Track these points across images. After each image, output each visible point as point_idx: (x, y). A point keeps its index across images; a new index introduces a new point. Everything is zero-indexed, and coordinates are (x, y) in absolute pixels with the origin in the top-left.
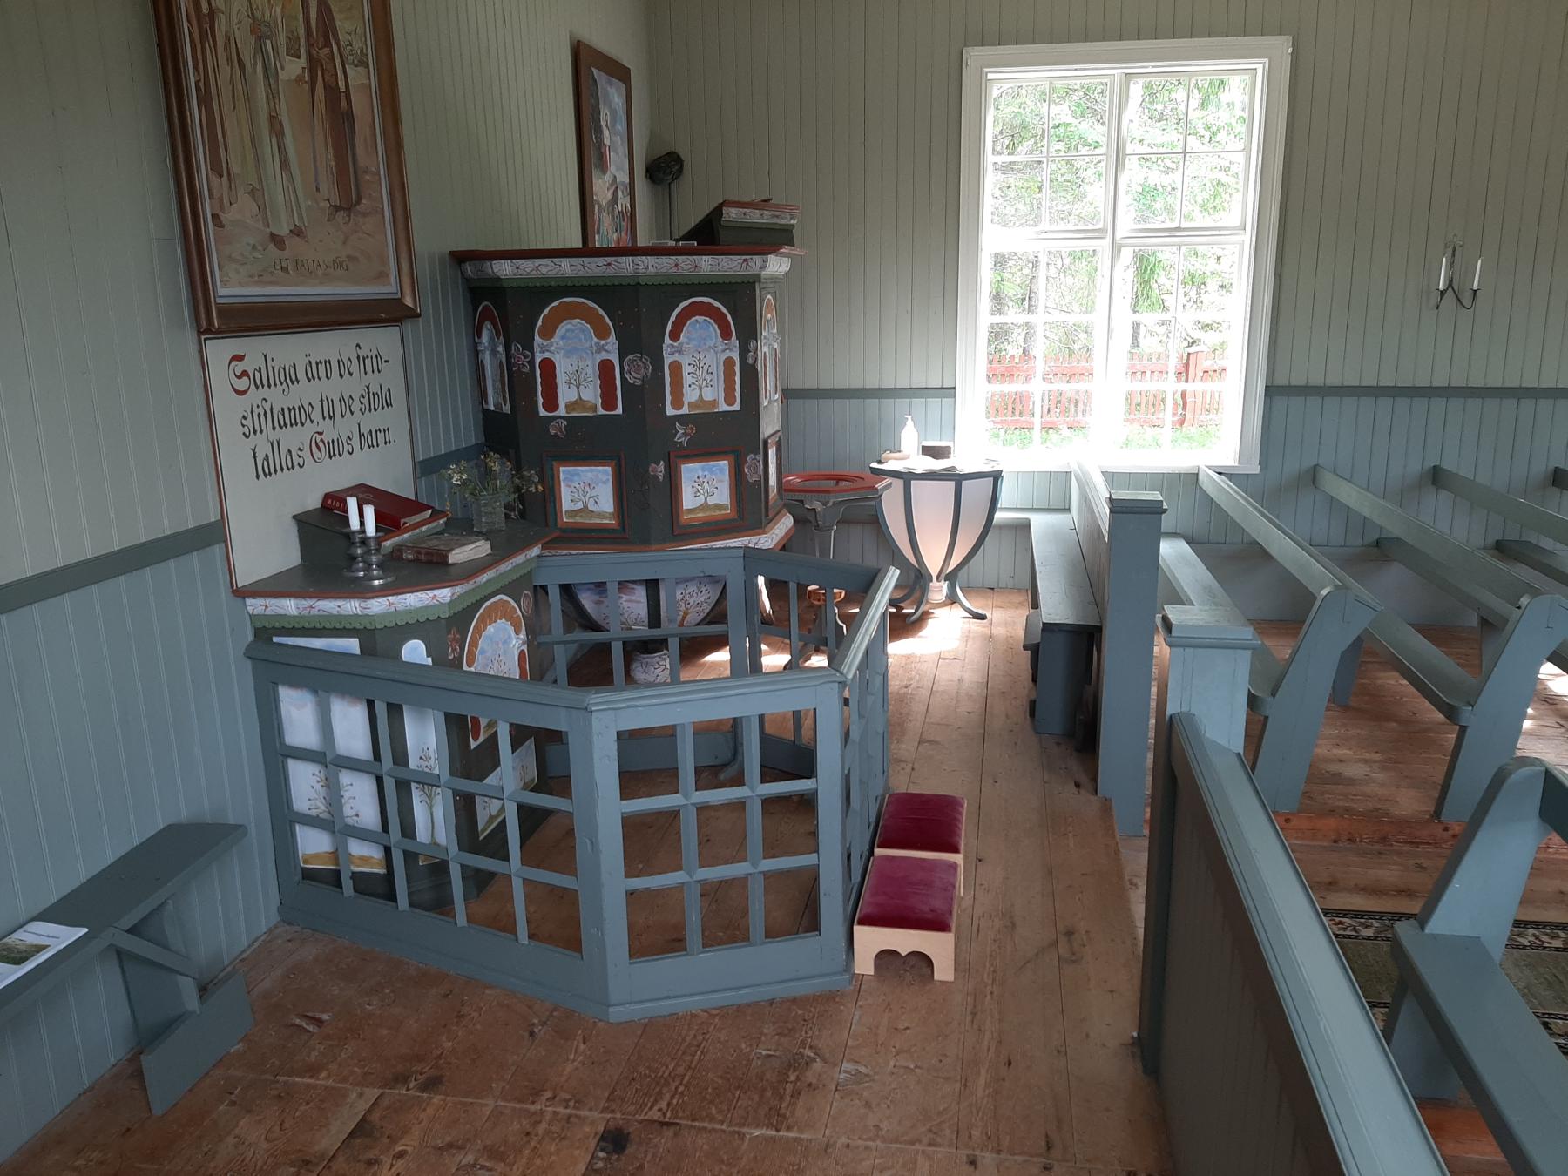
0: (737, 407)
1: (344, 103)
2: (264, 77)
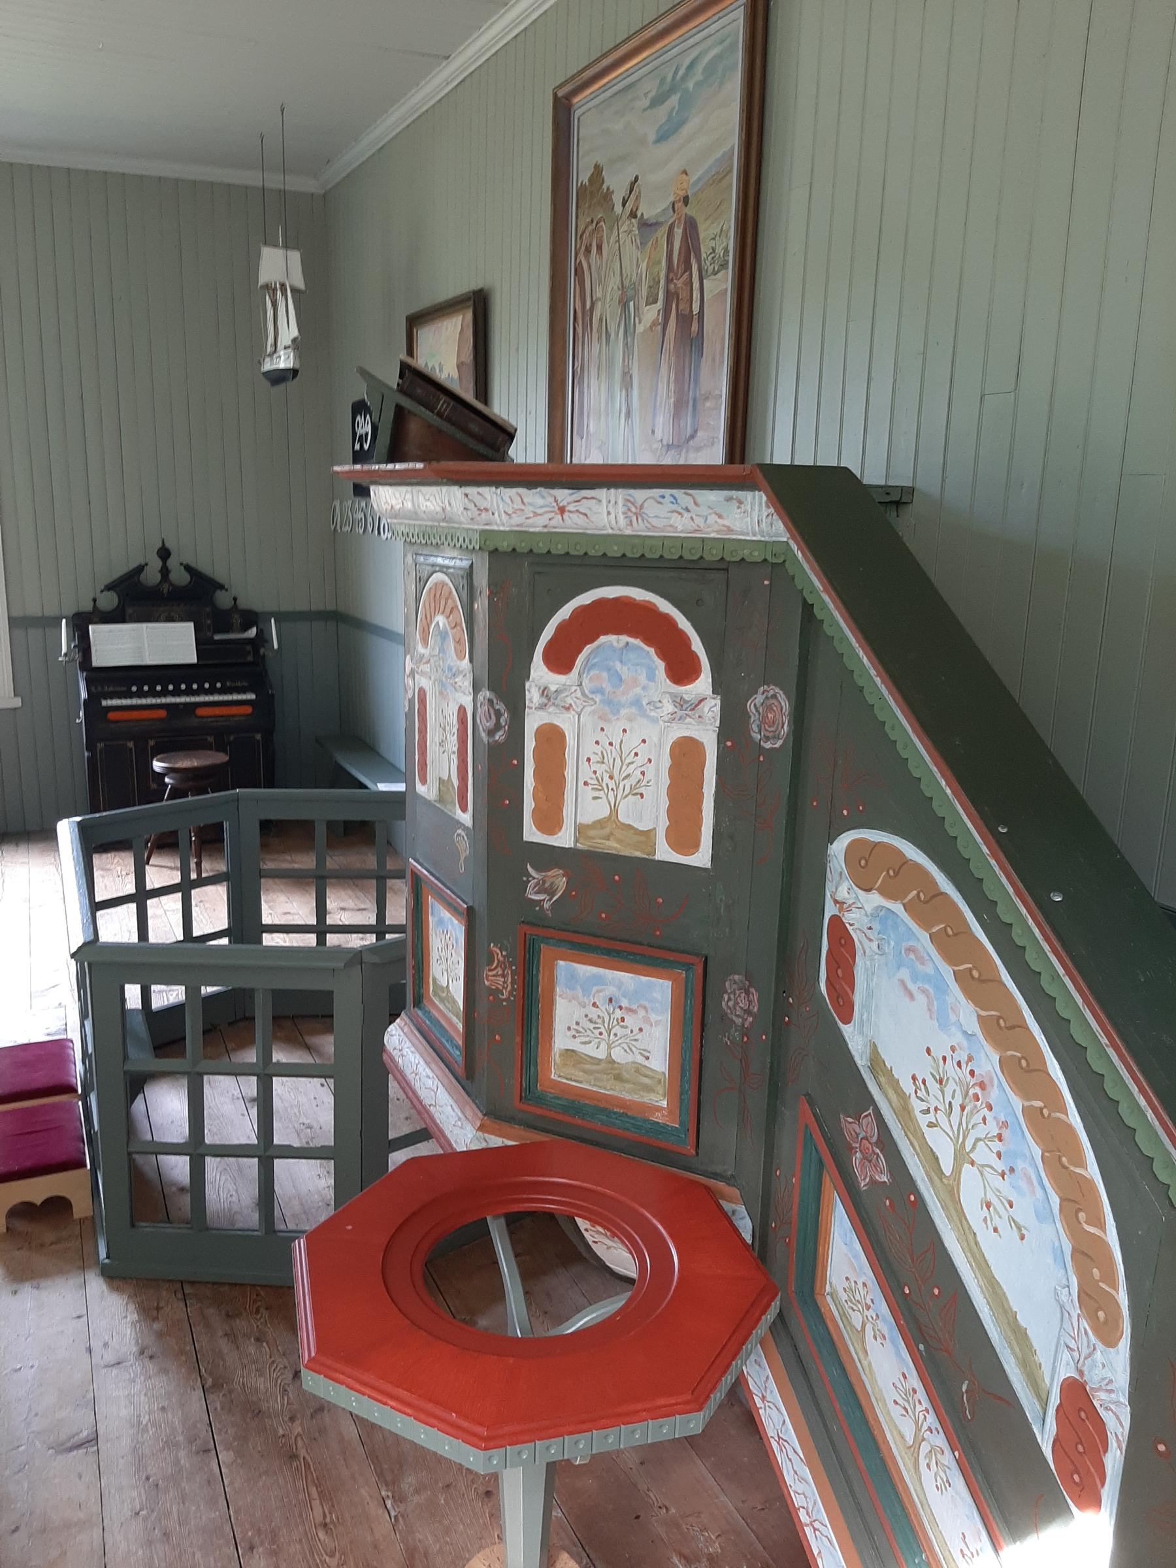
0: (702, 858)
1: (695, 327)
2: (624, 339)
